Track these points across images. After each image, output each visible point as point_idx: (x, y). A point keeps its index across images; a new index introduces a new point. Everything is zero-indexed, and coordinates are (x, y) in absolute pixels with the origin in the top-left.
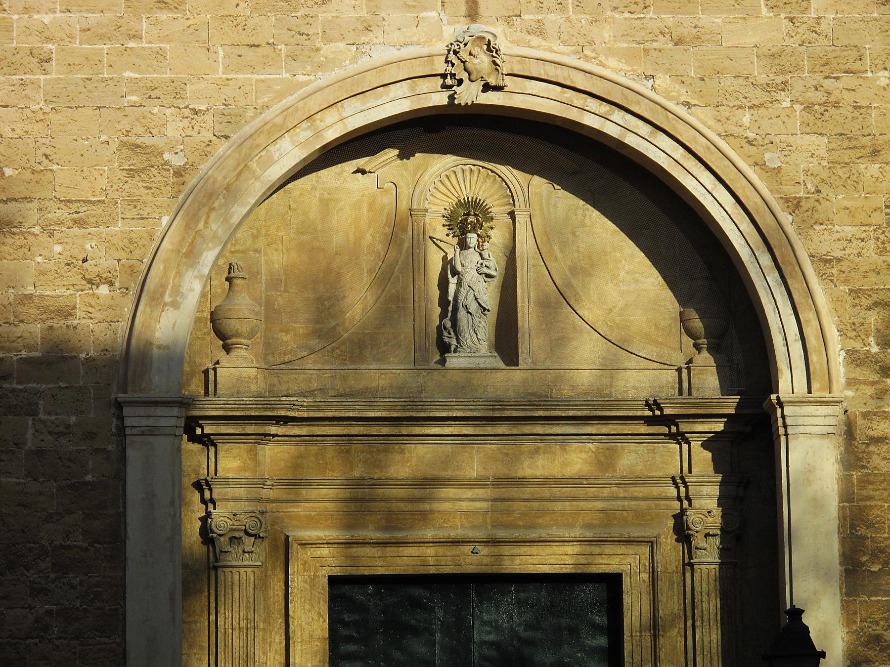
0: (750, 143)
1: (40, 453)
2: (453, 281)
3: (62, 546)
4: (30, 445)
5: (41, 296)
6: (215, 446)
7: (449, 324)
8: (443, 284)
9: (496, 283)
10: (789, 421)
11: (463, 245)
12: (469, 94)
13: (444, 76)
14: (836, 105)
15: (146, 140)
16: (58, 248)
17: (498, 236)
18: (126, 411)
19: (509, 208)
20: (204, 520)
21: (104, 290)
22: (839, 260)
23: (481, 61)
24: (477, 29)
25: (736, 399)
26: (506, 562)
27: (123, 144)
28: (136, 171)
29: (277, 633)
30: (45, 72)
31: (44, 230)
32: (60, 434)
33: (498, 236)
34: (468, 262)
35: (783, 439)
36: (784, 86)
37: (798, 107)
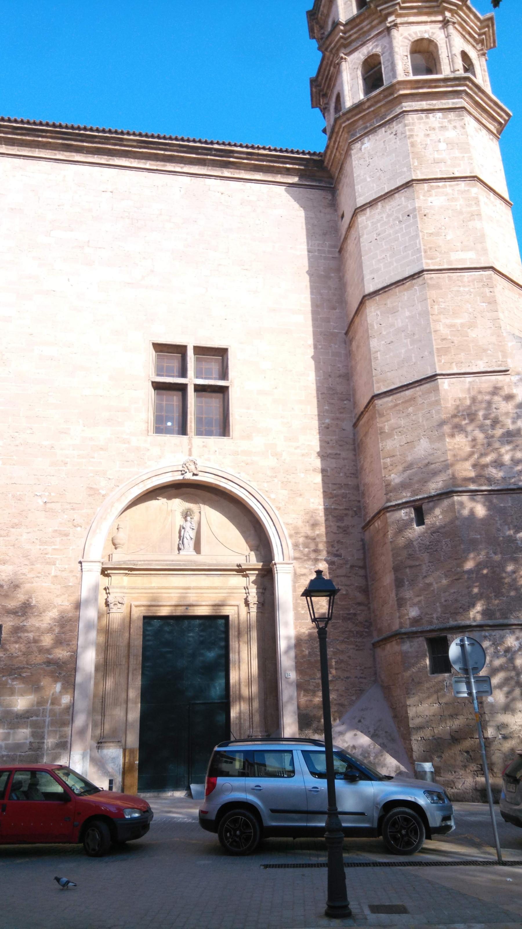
0: (267, 491)
1: (56, 576)
2: (183, 531)
3: (61, 605)
4: (53, 574)
5: (60, 530)
6: (111, 576)
7: (181, 542)
8: (180, 532)
9: (195, 531)
10: (278, 569)
11: (186, 521)
12: (189, 476)
13: (181, 471)
14: (290, 482)
15: (94, 486)
16: (66, 516)
17: (196, 518)
18: (83, 564)
19: (199, 511)
20: (106, 599)
21: (79, 529)
22: (291, 524)
23: (192, 467)
24: (191, 458)
25: (262, 564)
26: (196, 611)
27: (88, 487)
28: (91, 495)
29: (413, 158)
30: (66, 467)
31: (62, 511)
32: (63, 571)
33: (196, 518)
34: (188, 525)
35: (276, 574)
36: (276, 477)
37: (280, 482)
